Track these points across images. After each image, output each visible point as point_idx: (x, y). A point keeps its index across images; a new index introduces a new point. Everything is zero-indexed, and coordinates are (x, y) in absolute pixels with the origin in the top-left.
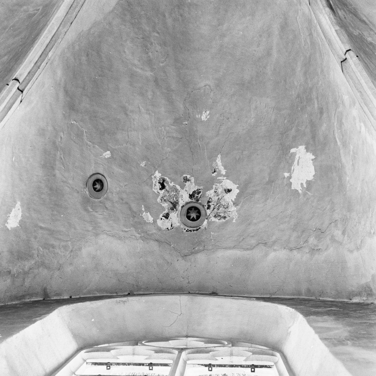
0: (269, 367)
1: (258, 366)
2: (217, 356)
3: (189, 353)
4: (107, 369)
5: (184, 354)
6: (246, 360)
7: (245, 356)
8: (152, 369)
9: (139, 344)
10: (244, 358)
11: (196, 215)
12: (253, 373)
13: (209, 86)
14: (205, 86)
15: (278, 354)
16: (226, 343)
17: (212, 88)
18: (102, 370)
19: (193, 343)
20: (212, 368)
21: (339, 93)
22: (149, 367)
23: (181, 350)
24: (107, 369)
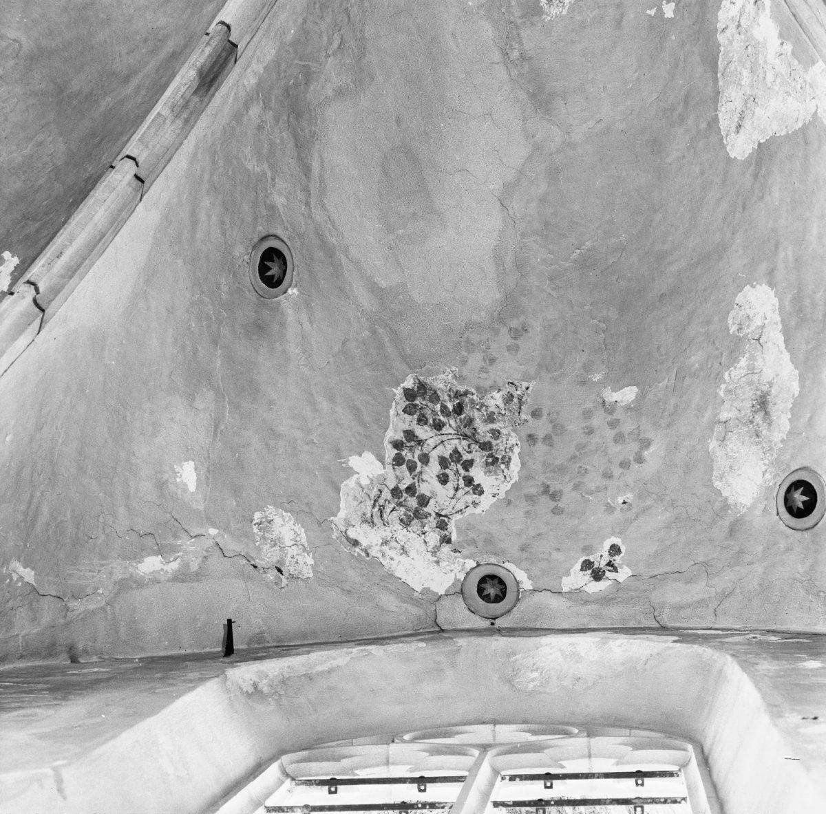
0: (671, 774)
1: (317, 785)
2: (561, 760)
3: (499, 755)
4: (329, 793)
5: (491, 753)
6: (411, 771)
7: (616, 758)
8: (551, 787)
9: (396, 740)
10: (614, 761)
11: (489, 594)
12: (423, 793)
13: (20, 47)
14: (15, 40)
15: (690, 747)
16: (576, 731)
17: (21, 52)
18: (320, 796)
19: (507, 733)
20: (425, 786)
21: (289, 122)
22: (419, 786)
23: (485, 748)
24: (329, 793)
